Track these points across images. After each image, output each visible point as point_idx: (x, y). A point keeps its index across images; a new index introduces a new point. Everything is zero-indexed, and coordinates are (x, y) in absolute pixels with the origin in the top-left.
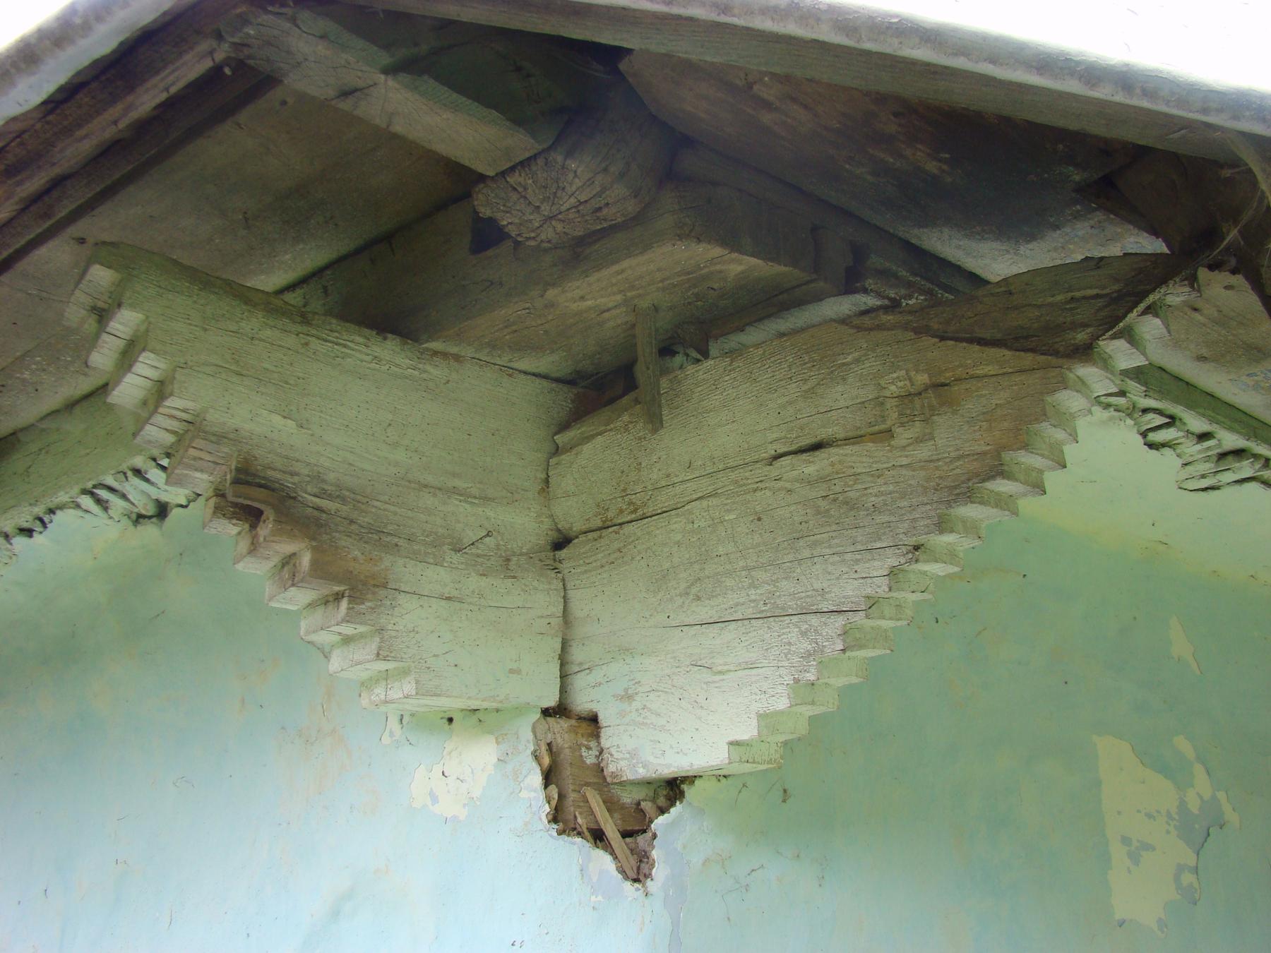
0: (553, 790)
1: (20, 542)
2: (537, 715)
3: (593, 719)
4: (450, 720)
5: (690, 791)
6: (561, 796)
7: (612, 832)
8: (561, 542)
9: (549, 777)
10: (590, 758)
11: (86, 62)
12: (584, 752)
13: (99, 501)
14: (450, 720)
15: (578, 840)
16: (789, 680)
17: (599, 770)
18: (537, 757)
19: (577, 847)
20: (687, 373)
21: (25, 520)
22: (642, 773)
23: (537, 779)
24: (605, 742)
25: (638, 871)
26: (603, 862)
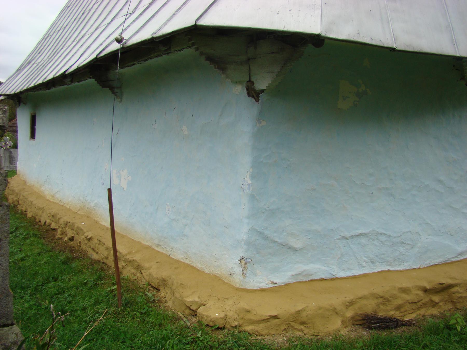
0: (248, 91)
1: (179, 52)
2: (246, 82)
3: (253, 82)
4: (237, 82)
5: (265, 91)
6: (249, 92)
7: (255, 96)
8: (249, 59)
9: (247, 90)
10: (253, 87)
11: (166, 33)
12: (252, 86)
13: (190, 48)
14: (237, 82)
15: (250, 97)
16: (271, 80)
17: (254, 88)
18: (246, 87)
19: (250, 98)
20: (17, 233)
21: (179, 49)
22: (258, 89)
23: (246, 90)
24: (255, 85)
25: (257, 101)
26: (253, 100)
